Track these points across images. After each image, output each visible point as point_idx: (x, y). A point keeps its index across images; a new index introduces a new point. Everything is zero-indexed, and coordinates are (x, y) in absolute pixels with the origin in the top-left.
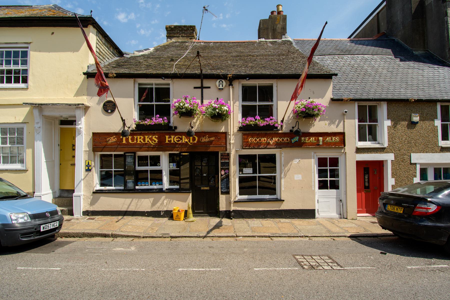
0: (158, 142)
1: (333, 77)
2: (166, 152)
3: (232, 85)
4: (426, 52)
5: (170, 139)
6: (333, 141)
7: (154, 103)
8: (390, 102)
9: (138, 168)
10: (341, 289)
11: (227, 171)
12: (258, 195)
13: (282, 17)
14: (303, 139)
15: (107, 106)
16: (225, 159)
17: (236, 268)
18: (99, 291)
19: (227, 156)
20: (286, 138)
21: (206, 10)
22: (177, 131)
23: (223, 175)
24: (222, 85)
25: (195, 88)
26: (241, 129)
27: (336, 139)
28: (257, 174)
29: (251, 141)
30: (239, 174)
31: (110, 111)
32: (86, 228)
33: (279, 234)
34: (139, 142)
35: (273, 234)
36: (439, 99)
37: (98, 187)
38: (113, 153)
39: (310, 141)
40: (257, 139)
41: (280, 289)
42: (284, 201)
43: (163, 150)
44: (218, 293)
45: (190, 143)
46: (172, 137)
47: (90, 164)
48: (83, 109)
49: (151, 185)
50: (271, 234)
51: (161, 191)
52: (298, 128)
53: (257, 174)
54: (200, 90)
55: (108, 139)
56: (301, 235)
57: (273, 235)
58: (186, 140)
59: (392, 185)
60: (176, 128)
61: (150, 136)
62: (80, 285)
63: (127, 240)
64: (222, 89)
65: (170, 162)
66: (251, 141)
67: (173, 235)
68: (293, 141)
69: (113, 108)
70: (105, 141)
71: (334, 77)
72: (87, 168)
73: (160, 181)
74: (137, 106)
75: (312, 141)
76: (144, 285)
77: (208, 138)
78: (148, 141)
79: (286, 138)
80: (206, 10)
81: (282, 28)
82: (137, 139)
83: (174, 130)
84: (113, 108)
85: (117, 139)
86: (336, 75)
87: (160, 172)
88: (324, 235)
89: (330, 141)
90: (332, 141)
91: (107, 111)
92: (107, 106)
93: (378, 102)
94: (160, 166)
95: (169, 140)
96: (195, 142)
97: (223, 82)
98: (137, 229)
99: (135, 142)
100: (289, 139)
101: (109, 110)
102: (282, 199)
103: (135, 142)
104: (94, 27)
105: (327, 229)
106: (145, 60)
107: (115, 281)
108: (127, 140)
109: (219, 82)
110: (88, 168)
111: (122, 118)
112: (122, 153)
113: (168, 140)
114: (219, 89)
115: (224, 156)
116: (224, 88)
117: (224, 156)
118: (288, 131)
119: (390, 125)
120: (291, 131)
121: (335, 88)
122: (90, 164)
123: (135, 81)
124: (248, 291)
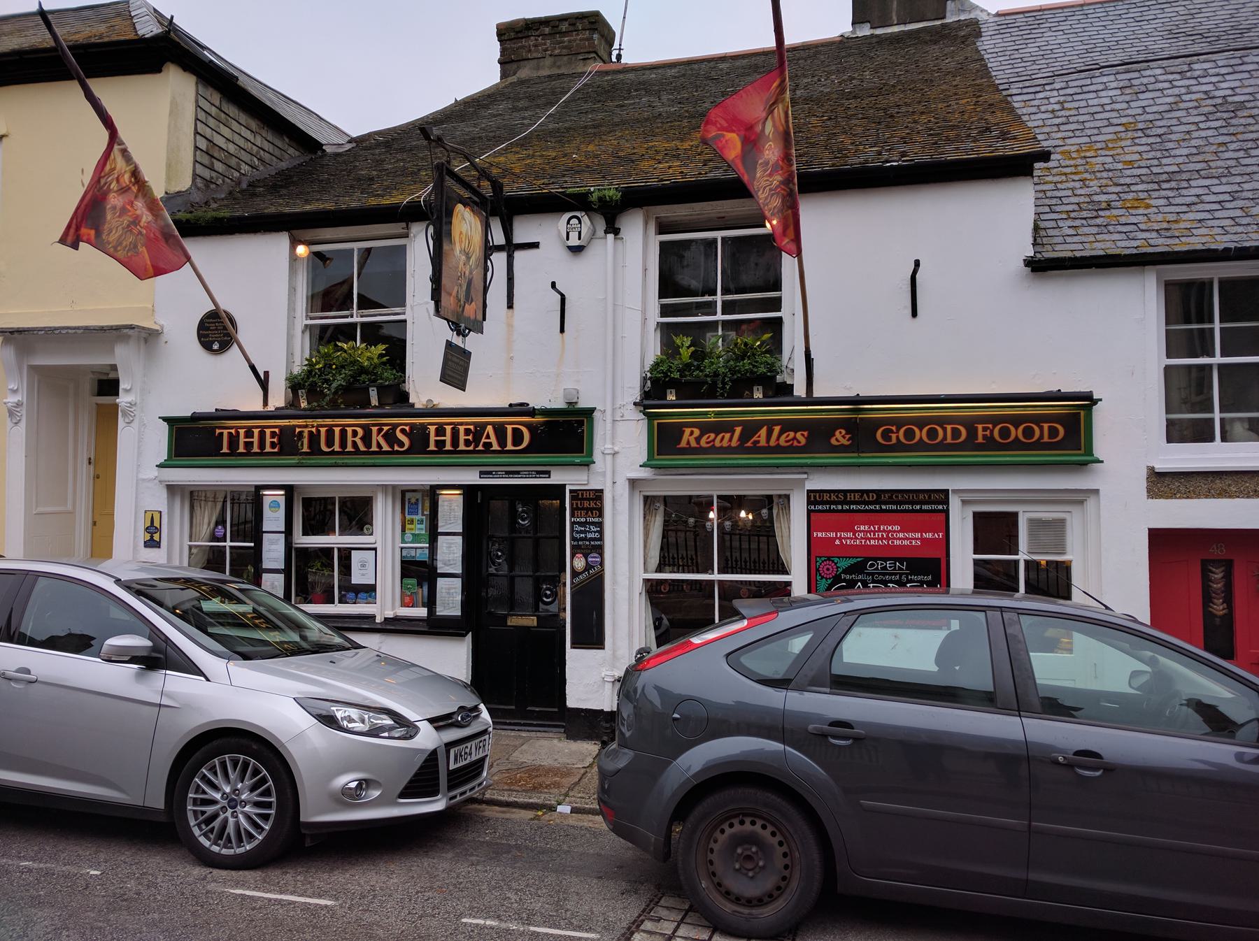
1: (1037, 165)
11: (593, 558)
15: (208, 329)
19: (593, 499)
24: (580, 233)
31: (216, 346)
97: (580, 222)
101: (213, 342)
109: (568, 223)
110: (152, 537)
114: (570, 248)
115: (583, 499)
117: (583, 499)
122: (156, 524)
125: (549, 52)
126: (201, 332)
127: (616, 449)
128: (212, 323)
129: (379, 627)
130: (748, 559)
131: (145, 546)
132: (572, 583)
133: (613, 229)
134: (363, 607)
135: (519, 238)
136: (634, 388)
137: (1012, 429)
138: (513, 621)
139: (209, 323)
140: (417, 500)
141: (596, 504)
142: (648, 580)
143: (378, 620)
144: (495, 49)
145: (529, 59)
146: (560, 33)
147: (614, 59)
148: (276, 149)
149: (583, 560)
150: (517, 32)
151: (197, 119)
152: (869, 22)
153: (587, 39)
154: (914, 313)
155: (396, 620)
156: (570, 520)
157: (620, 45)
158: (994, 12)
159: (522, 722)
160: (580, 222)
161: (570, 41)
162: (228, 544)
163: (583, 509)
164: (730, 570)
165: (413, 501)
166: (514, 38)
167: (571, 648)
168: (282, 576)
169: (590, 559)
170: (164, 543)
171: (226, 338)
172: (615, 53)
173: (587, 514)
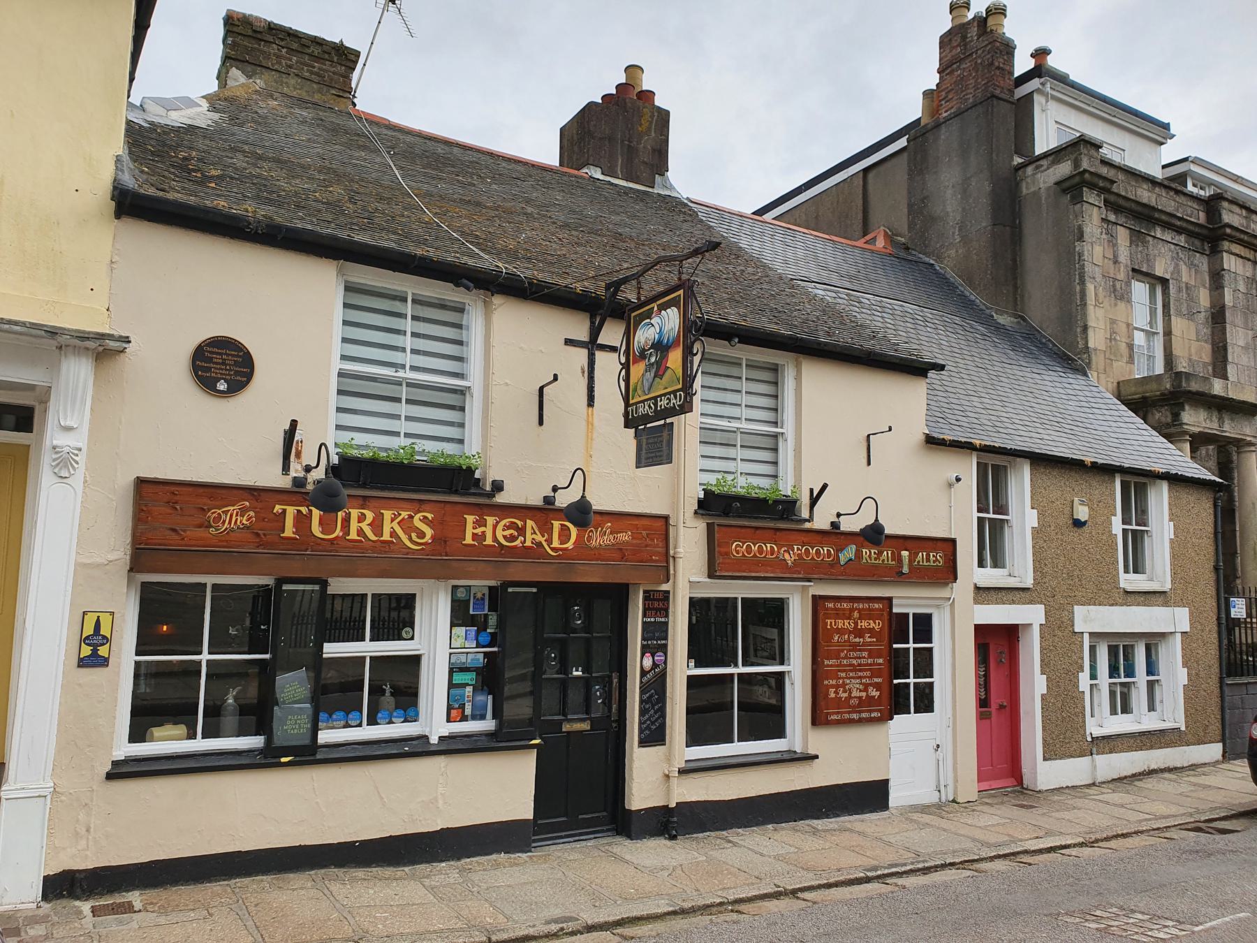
0: (433, 537)
4: (1019, 320)
5: (483, 529)
8: (1041, 461)
11: (659, 657)
13: (656, 114)
15: (210, 360)
19: (661, 600)
22: (500, 498)
25: (569, 342)
28: (736, 665)
30: (688, 667)
31: (222, 386)
34: (353, 535)
36: (1125, 465)
37: (125, 749)
38: (209, 580)
42: (817, 757)
45: (553, 549)
46: (490, 520)
48: (93, 354)
49: (372, 721)
51: (416, 748)
52: (877, 520)
54: (584, 353)
55: (212, 515)
58: (539, 538)
59: (1042, 695)
60: (498, 487)
61: (404, 514)
69: (237, 373)
70: (198, 521)
71: (931, 374)
72: (86, 651)
81: (654, 150)
82: (347, 520)
83: (491, 495)
84: (237, 373)
89: (925, 564)
90: (928, 563)
93: (1011, 458)
94: (412, 638)
95: (475, 531)
96: (570, 545)
99: (338, 532)
102: (812, 752)
103: (338, 532)
110: (95, 651)
119: (1037, 526)
122: (105, 631)
132: (641, 682)
135: (601, 340)
137: (752, 546)
138: (566, 727)
143: (434, 740)
149: (651, 659)
150: (255, 31)
154: (541, 423)
155: (128, 761)
156: (643, 620)
159: (563, 834)
165: (479, 595)
166: (250, 36)
169: (656, 658)
173: (656, 614)
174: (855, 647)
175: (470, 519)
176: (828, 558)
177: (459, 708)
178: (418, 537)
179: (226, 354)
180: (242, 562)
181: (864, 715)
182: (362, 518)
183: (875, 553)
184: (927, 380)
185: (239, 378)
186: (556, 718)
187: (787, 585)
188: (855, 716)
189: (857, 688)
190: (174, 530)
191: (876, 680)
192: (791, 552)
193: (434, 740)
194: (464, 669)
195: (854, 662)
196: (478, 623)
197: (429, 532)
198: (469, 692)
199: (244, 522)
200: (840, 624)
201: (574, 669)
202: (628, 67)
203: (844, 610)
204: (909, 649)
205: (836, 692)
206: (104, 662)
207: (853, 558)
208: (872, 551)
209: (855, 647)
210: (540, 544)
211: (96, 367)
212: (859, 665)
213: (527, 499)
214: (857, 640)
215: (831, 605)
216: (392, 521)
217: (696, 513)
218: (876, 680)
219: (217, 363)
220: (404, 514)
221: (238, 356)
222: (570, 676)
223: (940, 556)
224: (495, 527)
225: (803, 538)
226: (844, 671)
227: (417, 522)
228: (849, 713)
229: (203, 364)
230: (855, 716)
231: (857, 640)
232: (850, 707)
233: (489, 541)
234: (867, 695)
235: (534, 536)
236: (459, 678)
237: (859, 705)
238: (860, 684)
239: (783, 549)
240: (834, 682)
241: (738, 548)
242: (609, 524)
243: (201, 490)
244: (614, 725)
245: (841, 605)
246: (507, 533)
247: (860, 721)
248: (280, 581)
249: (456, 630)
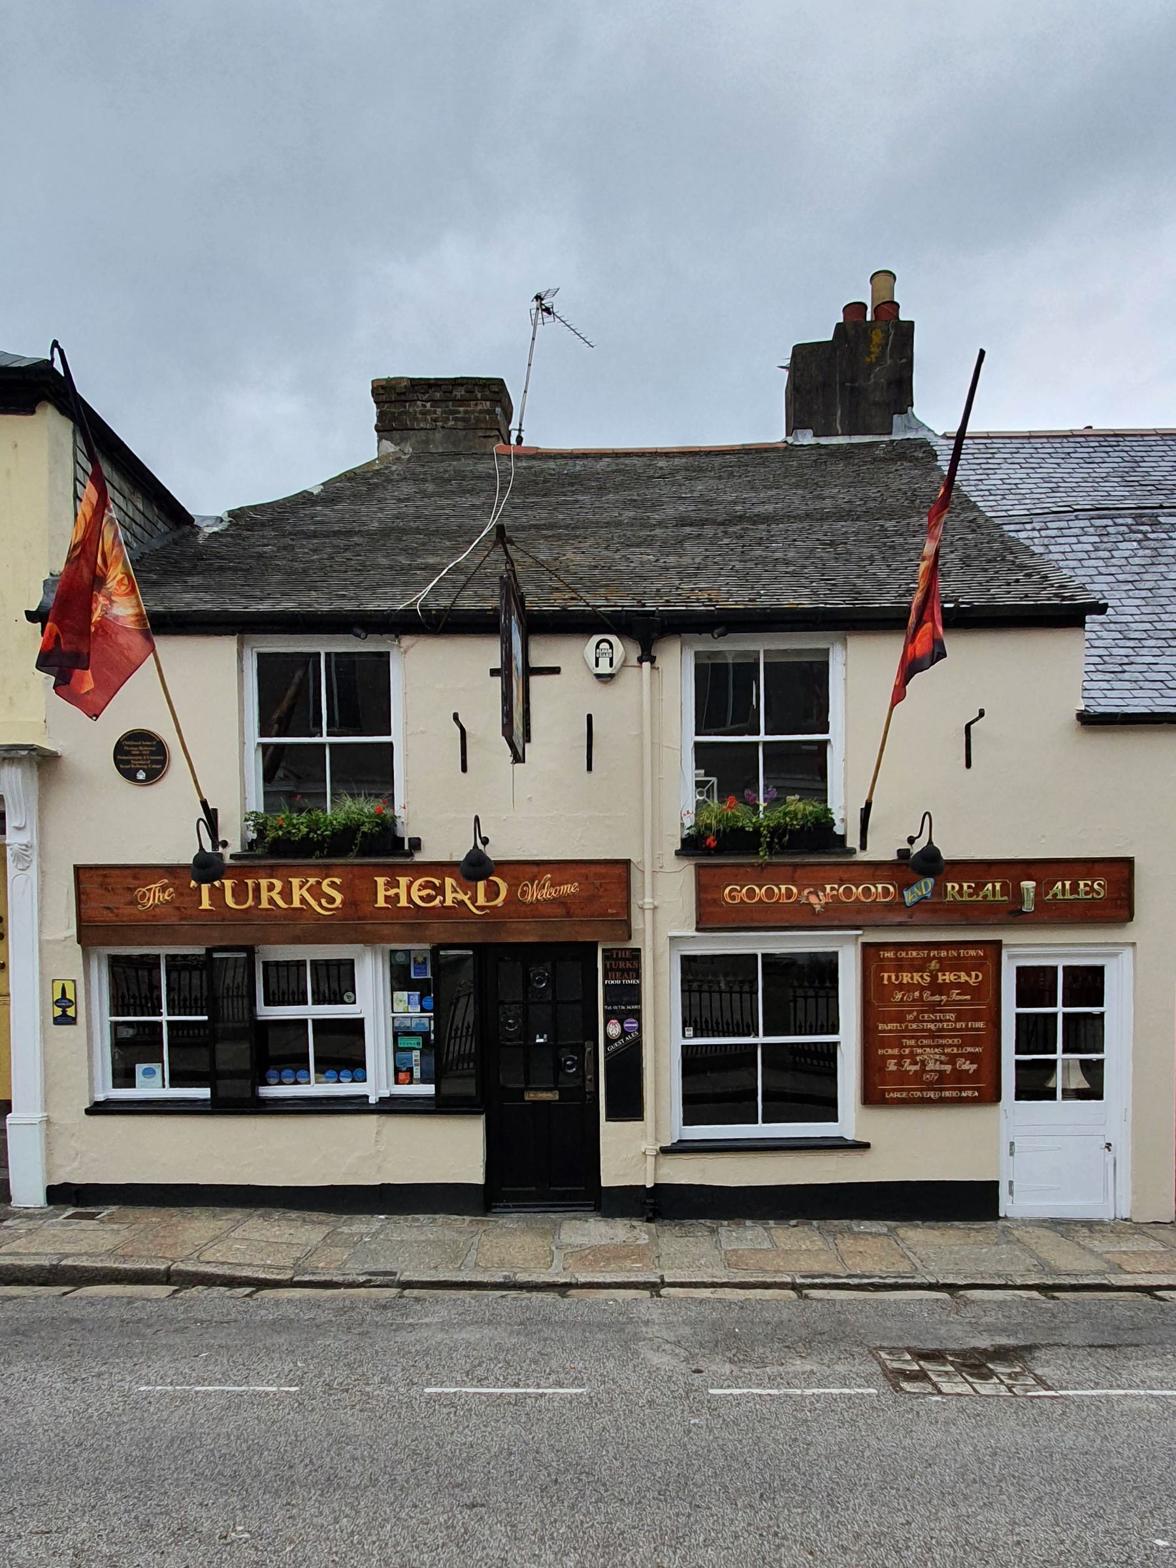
0: (343, 902)
1: (1088, 618)
2: (379, 946)
3: (652, 660)
6: (1082, 896)
7: (325, 739)
8: (40, 932)
9: (269, 1013)
10: (1019, 1458)
11: (630, 1024)
12: (764, 1122)
14: (953, 887)
15: (128, 753)
16: (625, 972)
17: (642, 1388)
18: (134, 1454)
19: (628, 959)
20: (880, 886)
21: (547, 310)
22: (419, 858)
23: (616, 1040)
24: (611, 660)
26: (691, 846)
27: (1096, 886)
29: (733, 898)
31: (141, 775)
32: (67, 1249)
33: (835, 1277)
34: (265, 904)
35: (813, 1277)
38: (163, 951)
39: (980, 898)
40: (854, 889)
41: (794, 1454)
43: (368, 939)
44: (564, 1463)
45: (478, 908)
46: (403, 881)
47: (68, 997)
50: (803, 1277)
51: (356, 1106)
52: (930, 842)
53: (757, 1035)
56: (926, 1281)
57: (809, 1281)
58: (461, 896)
61: (312, 881)
62: (62, 1434)
63: (228, 1293)
64: (611, 676)
65: (393, 990)
66: (733, 898)
67: (406, 1276)
68: (909, 897)
72: (58, 1012)
73: (355, 1065)
74: (256, 750)
75: (990, 894)
76: (296, 1436)
77: (552, 886)
78: (303, 900)
79: (880, 886)
80: (547, 310)
81: (889, 383)
82: (257, 889)
83: (410, 855)
85: (748, 832)
86: (1101, 609)
87: (355, 1027)
88: (1019, 1282)
89: (1068, 896)
91: (129, 774)
92: (128, 753)
94: (354, 1002)
95: (388, 893)
96: (499, 902)
97: (611, 647)
98: (269, 1256)
99: (250, 902)
100: (892, 889)
101: (137, 770)
103: (250, 902)
104: (64, 410)
105: (1038, 1258)
106: (285, 548)
107: (187, 1424)
108: (217, 895)
109: (597, 647)
110: (64, 1012)
111: (204, 804)
112: (200, 950)
113: (386, 897)
114: (598, 676)
115: (618, 959)
116: (620, 670)
117: (618, 959)
118: (892, 856)
120: (903, 854)
121: (1105, 663)
122: (70, 995)
123: (241, 644)
124: (672, 1459)
125: (441, 424)
126: (119, 757)
127: (656, 903)
128: (135, 746)
129: (372, 1108)
130: (730, 1021)
131: (55, 1024)
132: (606, 1051)
133: (647, 656)
134: (347, 1087)
136: (673, 836)
138: (530, 1096)
139: (129, 746)
140: (425, 959)
141: (632, 964)
142: (687, 1046)
143: (372, 1100)
144: (371, 412)
145: (414, 429)
146: (454, 400)
147: (513, 441)
148: (147, 522)
151: (76, 479)
152: (812, 428)
153: (488, 412)
154: (968, 765)
157: (521, 425)
158: (940, 433)
160: (611, 647)
161: (466, 412)
162: (165, 1018)
163: (618, 970)
164: (710, 1033)
165: (420, 959)
167: (607, 1120)
168: (272, 1052)
169: (626, 1025)
170: (81, 1019)
171: (154, 766)
172: (514, 435)
173: (622, 976)
174: (933, 1008)
175: (381, 881)
176: (885, 897)
177: (407, 1071)
178: (328, 903)
179: (142, 745)
180: (167, 933)
181: (947, 1094)
182: (271, 888)
183: (969, 887)
184: (1088, 635)
185: (154, 766)
186: (517, 1086)
187: (713, 937)
188: (931, 1094)
189: (936, 1060)
190: (108, 908)
191: (970, 1049)
192: (821, 894)
193: (372, 1100)
194: (409, 1033)
195: (931, 1026)
196: (422, 988)
197: (339, 897)
198: (416, 1056)
199: (166, 898)
200: (906, 978)
201: (538, 1036)
202: (891, 273)
203: (913, 959)
204: (1055, 1015)
205: (899, 1064)
206: (73, 1021)
207: (929, 895)
208: (965, 885)
209: (933, 1008)
210: (462, 903)
211: (41, 778)
212: (939, 1030)
213: (451, 855)
214: (937, 998)
215: (890, 955)
216: (301, 887)
217: (677, 853)
218: (970, 1049)
219: (134, 755)
220: (312, 881)
221: (151, 746)
222: (530, 1043)
223: (1099, 884)
224: (409, 888)
225: (840, 873)
226: (912, 1037)
227: (325, 887)
228: (921, 1090)
229: (124, 758)
230: (931, 1094)
231: (937, 998)
232: (923, 1083)
233: (403, 903)
234: (954, 1069)
235: (455, 895)
236: (404, 1042)
237: (940, 1081)
238: (941, 1054)
239: (806, 892)
240: (896, 1051)
241: (734, 893)
242: (549, 876)
243: (128, 871)
244: (588, 1097)
245: (907, 954)
246: (424, 893)
247: (942, 1102)
248: (209, 951)
249: (397, 994)
